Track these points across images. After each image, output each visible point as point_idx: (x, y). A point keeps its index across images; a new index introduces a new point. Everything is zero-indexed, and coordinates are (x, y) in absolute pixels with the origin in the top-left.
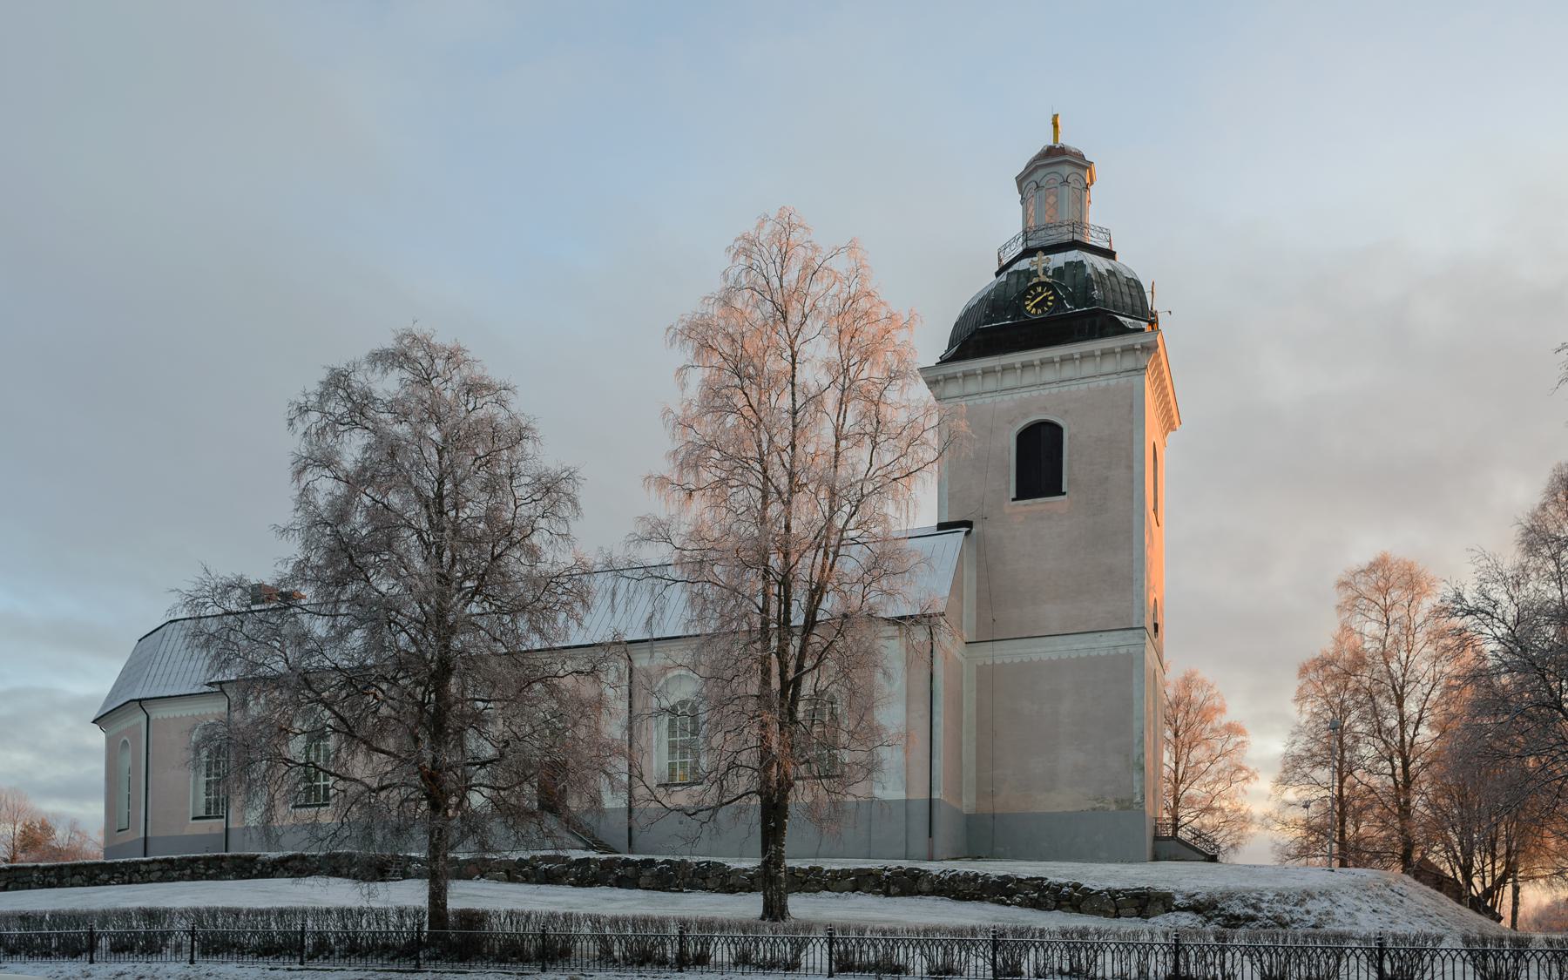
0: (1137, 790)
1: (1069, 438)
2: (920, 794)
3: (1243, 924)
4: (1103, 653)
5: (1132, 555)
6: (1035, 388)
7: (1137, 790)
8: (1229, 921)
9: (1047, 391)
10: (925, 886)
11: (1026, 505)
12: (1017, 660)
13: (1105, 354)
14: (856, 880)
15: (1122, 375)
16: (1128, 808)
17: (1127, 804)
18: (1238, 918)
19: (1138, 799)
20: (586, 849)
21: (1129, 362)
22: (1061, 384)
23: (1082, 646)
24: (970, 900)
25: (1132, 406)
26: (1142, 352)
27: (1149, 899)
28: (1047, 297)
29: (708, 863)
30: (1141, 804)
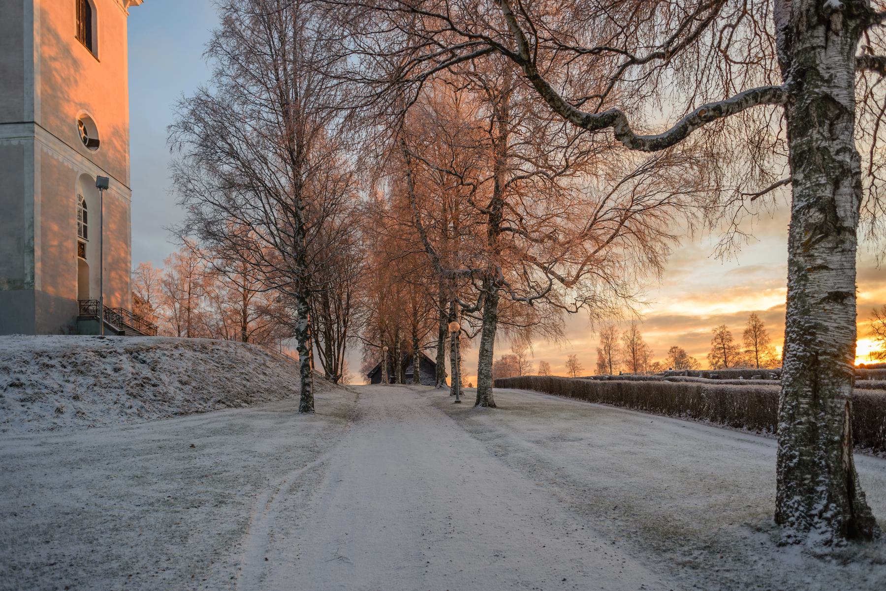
5: (22, 56)
7: (28, 271)
19: (28, 279)
30: (32, 284)
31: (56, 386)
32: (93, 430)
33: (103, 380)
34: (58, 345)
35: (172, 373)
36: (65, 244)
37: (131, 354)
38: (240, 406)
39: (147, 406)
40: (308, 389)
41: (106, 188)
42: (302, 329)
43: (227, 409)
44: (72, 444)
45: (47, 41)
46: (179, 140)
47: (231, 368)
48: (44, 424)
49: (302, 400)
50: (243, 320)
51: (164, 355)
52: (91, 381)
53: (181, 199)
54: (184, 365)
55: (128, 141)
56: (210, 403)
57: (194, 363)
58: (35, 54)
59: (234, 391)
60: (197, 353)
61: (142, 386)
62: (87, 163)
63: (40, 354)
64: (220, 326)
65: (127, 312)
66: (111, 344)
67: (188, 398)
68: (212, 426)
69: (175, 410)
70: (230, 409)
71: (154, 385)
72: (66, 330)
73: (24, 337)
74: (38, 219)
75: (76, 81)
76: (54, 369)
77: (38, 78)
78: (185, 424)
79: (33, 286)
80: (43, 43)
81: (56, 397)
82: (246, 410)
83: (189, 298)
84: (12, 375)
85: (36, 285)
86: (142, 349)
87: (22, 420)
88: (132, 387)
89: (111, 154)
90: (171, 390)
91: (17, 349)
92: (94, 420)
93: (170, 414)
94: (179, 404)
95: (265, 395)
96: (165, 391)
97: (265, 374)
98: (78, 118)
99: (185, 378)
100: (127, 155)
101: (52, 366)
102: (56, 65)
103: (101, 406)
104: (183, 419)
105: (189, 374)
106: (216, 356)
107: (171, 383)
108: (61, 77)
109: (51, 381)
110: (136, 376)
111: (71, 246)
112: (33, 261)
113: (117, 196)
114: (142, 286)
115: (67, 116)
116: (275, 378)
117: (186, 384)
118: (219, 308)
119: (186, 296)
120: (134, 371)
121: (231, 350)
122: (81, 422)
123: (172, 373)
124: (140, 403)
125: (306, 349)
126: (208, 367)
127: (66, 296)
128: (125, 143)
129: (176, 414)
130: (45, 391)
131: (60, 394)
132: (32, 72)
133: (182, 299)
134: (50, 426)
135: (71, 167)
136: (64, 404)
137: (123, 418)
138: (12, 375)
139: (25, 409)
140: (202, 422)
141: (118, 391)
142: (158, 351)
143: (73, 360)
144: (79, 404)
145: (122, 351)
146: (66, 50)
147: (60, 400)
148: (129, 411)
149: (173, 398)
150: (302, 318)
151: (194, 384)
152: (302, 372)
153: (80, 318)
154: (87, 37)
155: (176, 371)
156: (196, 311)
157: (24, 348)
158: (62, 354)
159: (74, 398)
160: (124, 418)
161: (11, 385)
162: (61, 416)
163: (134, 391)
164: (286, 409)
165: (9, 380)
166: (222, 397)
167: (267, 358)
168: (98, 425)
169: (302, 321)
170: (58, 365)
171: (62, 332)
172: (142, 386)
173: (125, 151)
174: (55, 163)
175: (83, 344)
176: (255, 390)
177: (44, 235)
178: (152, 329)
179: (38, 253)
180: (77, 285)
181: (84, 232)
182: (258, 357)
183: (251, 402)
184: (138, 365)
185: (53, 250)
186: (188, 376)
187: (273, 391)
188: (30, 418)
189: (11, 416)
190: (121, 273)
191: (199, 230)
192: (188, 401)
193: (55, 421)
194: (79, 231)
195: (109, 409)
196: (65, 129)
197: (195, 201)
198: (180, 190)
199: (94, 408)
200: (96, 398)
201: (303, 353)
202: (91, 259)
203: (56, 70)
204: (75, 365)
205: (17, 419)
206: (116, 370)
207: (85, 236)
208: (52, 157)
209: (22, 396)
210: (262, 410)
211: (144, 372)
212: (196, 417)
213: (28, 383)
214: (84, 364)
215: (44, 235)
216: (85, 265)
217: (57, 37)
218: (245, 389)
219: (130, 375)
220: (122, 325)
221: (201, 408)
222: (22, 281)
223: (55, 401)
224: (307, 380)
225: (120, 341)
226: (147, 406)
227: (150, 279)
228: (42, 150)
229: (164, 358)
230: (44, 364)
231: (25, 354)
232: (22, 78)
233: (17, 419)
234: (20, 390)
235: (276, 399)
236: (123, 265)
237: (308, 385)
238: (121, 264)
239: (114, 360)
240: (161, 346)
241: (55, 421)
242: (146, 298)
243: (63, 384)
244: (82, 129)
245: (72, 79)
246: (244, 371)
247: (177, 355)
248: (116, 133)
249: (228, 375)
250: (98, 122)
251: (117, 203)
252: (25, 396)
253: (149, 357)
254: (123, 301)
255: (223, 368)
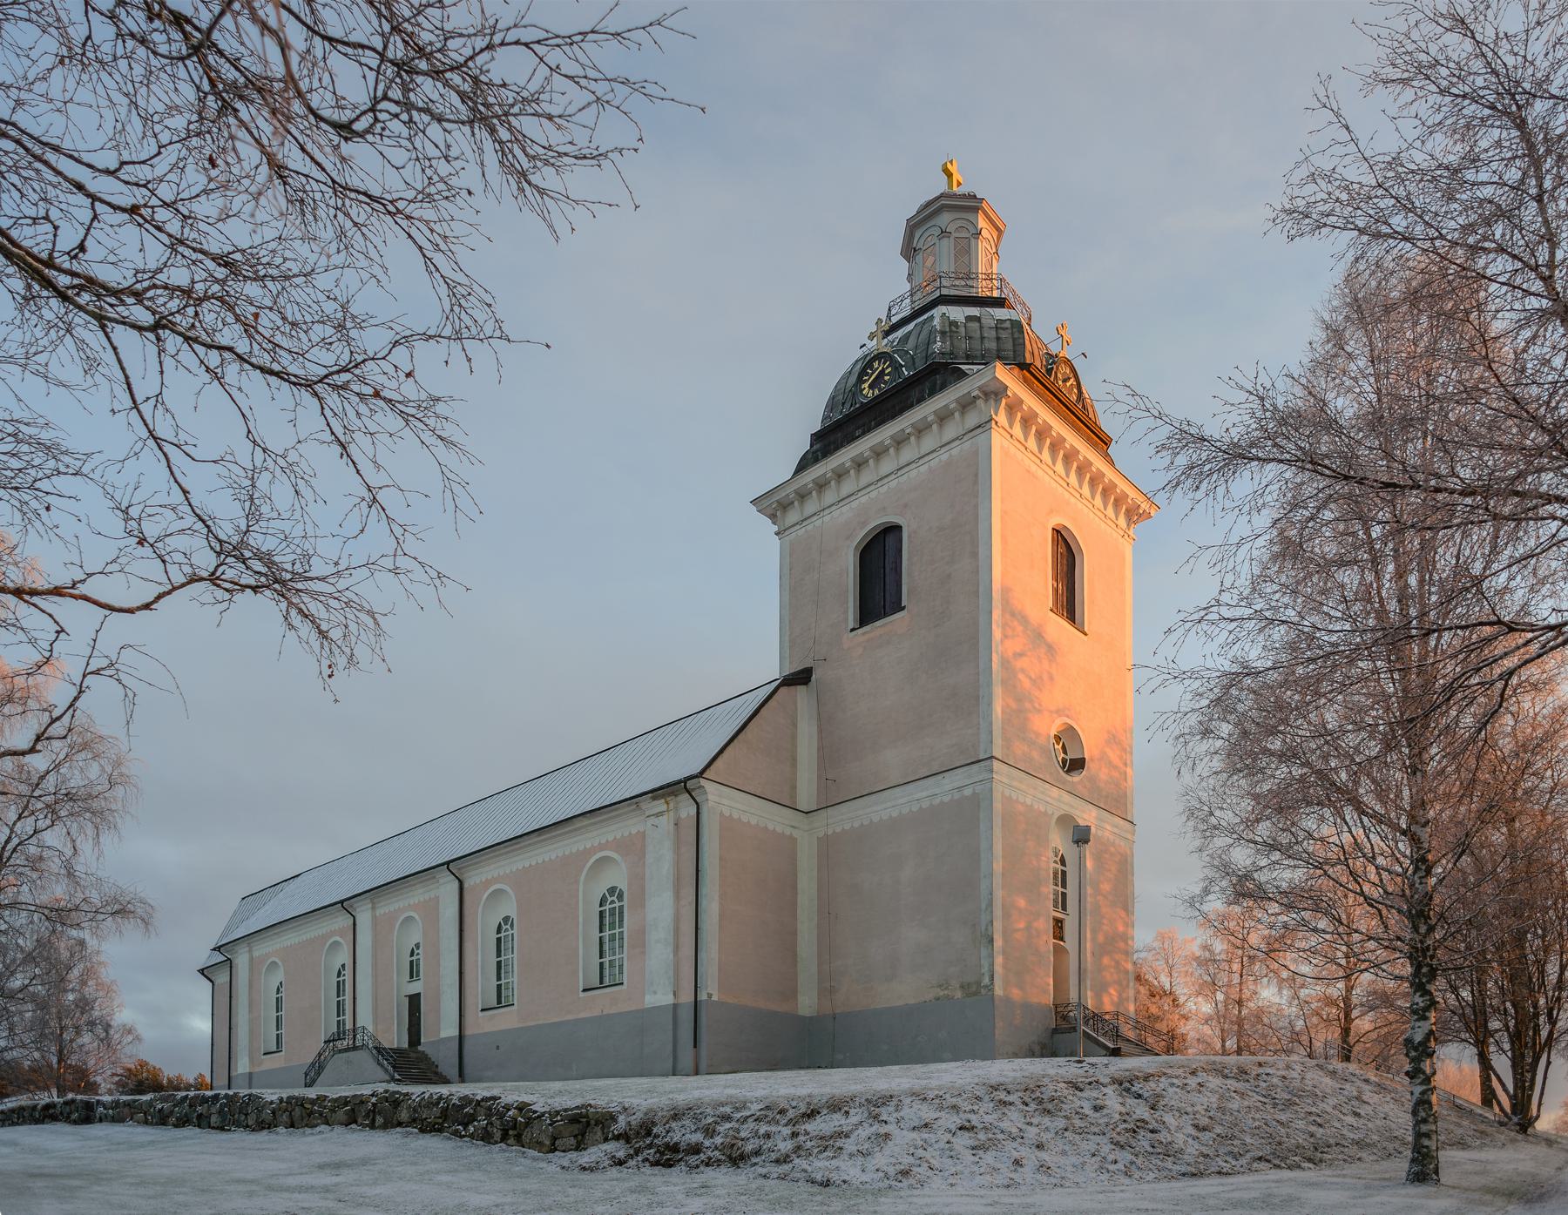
0: (985, 969)
1: (909, 537)
2: (687, 998)
3: (681, 1160)
4: (946, 799)
5: (978, 666)
6: (873, 487)
7: (985, 969)
8: (662, 1154)
9: (886, 487)
10: (404, 1115)
11: (864, 634)
12: (856, 825)
13: (943, 417)
14: (353, 1110)
15: (965, 438)
16: (976, 993)
17: (974, 989)
18: (675, 1148)
19: (986, 981)
20: (389, 1082)
21: (972, 419)
22: (900, 473)
23: (924, 794)
24: (431, 1131)
25: (976, 475)
26: (986, 401)
27: (588, 1123)
28: (883, 370)
29: (250, 1095)
30: (991, 987)
31: (1014, 1130)
32: (1060, 1190)
33: (1078, 1123)
34: (1019, 1074)
35: (1182, 1113)
36: (1035, 924)
37: (1121, 1084)
38: (1299, 1167)
39: (1139, 1161)
40: (1426, 1142)
41: (1087, 841)
42: (1418, 1038)
43: (1273, 1171)
44: (1030, 1206)
45: (1010, 633)
46: (1193, 755)
47: (1289, 1104)
48: (1000, 1180)
49: (1413, 1161)
50: (1342, 1016)
51: (1172, 1085)
52: (1061, 1123)
53: (1198, 843)
54: (1208, 1100)
55: (1131, 748)
56: (1243, 1161)
57: (1222, 1097)
58: (994, 655)
59: (1290, 1143)
60: (1229, 1082)
61: (1135, 1132)
62: (1067, 797)
63: (995, 1088)
64: (1297, 1029)
65: (1127, 1017)
66: (1091, 1071)
67: (1206, 1152)
68: (1236, 1195)
69: (1184, 1169)
70: (1278, 1171)
71: (1152, 1131)
72: (1037, 1049)
73: (979, 1063)
74: (999, 894)
75: (1051, 678)
76: (1012, 1108)
77: (998, 691)
78: (1192, 1190)
79: (992, 990)
80: (1005, 636)
81: (1015, 1145)
82: (1310, 1174)
83: (1241, 984)
84: (961, 1115)
85: (996, 988)
86: (1137, 1077)
87: (973, 1173)
88: (1119, 1134)
89: (1103, 775)
90: (1180, 1139)
91: (968, 1080)
92: (1063, 1178)
93: (1174, 1174)
94: (1191, 1160)
95: (1353, 1151)
96: (1169, 1139)
97: (1357, 1115)
98: (1053, 732)
99: (1204, 1121)
100: (1129, 770)
101: (1011, 1104)
102: (1020, 664)
103: (1074, 1159)
104: (1194, 1182)
105: (1211, 1114)
106: (1264, 1085)
107: (1179, 1128)
108: (1031, 678)
109: (1009, 1123)
110: (1126, 1117)
111: (1045, 926)
112: (991, 956)
113: (1112, 837)
114: (1160, 968)
115: (1038, 735)
116: (1378, 1122)
117: (1204, 1129)
118: (1296, 996)
119: (1236, 979)
120: (1123, 1110)
121: (1295, 1074)
122: (1045, 1179)
123: (1182, 1113)
124: (1130, 1157)
125: (1424, 1073)
126: (1246, 1103)
127: (1035, 1000)
128: (1125, 750)
129: (1184, 1175)
130: (1000, 1136)
131: (1019, 1140)
132: (990, 684)
133: (1229, 985)
134: (1006, 1182)
135: (1043, 809)
136: (1024, 1154)
137: (1102, 1177)
138: (961, 1115)
139: (977, 1159)
140: (1221, 1188)
141: (1098, 1139)
142: (1163, 1079)
143: (1038, 1094)
144: (1043, 1155)
145: (1107, 1080)
146: (1038, 636)
147: (1020, 1148)
148: (1112, 1167)
149: (1181, 1151)
150: (1418, 1020)
151: (1218, 1130)
152: (1414, 1113)
153: (1055, 1031)
154: (1069, 605)
155: (1189, 1109)
156: (1251, 1005)
157: (976, 1080)
158: (1023, 1087)
159: (1038, 1147)
160: (1105, 1176)
161: (960, 1129)
162: (1020, 1169)
163: (1122, 1139)
164: (1387, 1176)
165: (959, 1121)
166: (1267, 1151)
167: (1366, 1087)
168: (1068, 1184)
169: (1418, 1024)
170: (1018, 1102)
171: (1031, 1054)
172: (1135, 1132)
173: (1126, 764)
174: (1021, 808)
175: (1052, 1072)
176: (1332, 1141)
177: (1006, 915)
178: (1172, 1044)
179: (998, 942)
180: (1052, 983)
181: (1062, 901)
182: (1348, 1086)
183: (1321, 1161)
184: (1131, 1101)
185: (1018, 936)
186: (1210, 1117)
187: (1368, 1145)
188: (982, 1170)
189: (959, 1168)
190: (1117, 957)
191: (1223, 890)
192: (1206, 1156)
193: (1012, 1175)
194: (1056, 901)
195: (1084, 1164)
196: (1035, 755)
197: (1221, 841)
198: (1195, 829)
199: (1062, 1160)
200: (1066, 1148)
201: (1419, 1081)
202: (1070, 943)
203: (1023, 670)
204: (1040, 1101)
205: (966, 1172)
206: (1097, 1109)
207: (1064, 908)
208: (1017, 801)
209: (973, 1143)
210: (1338, 1176)
211: (1138, 1112)
212: (1216, 1180)
213: (980, 1126)
214: (1052, 1100)
215: (1006, 915)
216: (1064, 950)
217: (1024, 620)
218: (1312, 1140)
219: (1117, 1116)
220: (1117, 1035)
221: (1226, 1167)
222: (978, 983)
223: (1012, 1150)
224: (1424, 1128)
225: (1106, 1066)
226: (1139, 1161)
227: (1174, 956)
228: (1003, 793)
229: (1171, 1090)
230: (1000, 1101)
231: (977, 1087)
232: (977, 698)
233: (966, 1172)
234: (972, 1134)
235: (1375, 1158)
236: (1122, 945)
237: (1427, 1135)
238: (1118, 943)
239: (1095, 1094)
240: (1169, 1071)
241: (1012, 1175)
242: (1167, 987)
243: (1024, 1127)
244: (1058, 747)
245: (1045, 677)
246: (1314, 1109)
247: (1194, 1085)
248: (1114, 739)
249: (1283, 1117)
250: (1083, 731)
251: (1112, 849)
252: (977, 1143)
253: (1147, 1089)
254: (1122, 1000)
255: (1275, 1106)
